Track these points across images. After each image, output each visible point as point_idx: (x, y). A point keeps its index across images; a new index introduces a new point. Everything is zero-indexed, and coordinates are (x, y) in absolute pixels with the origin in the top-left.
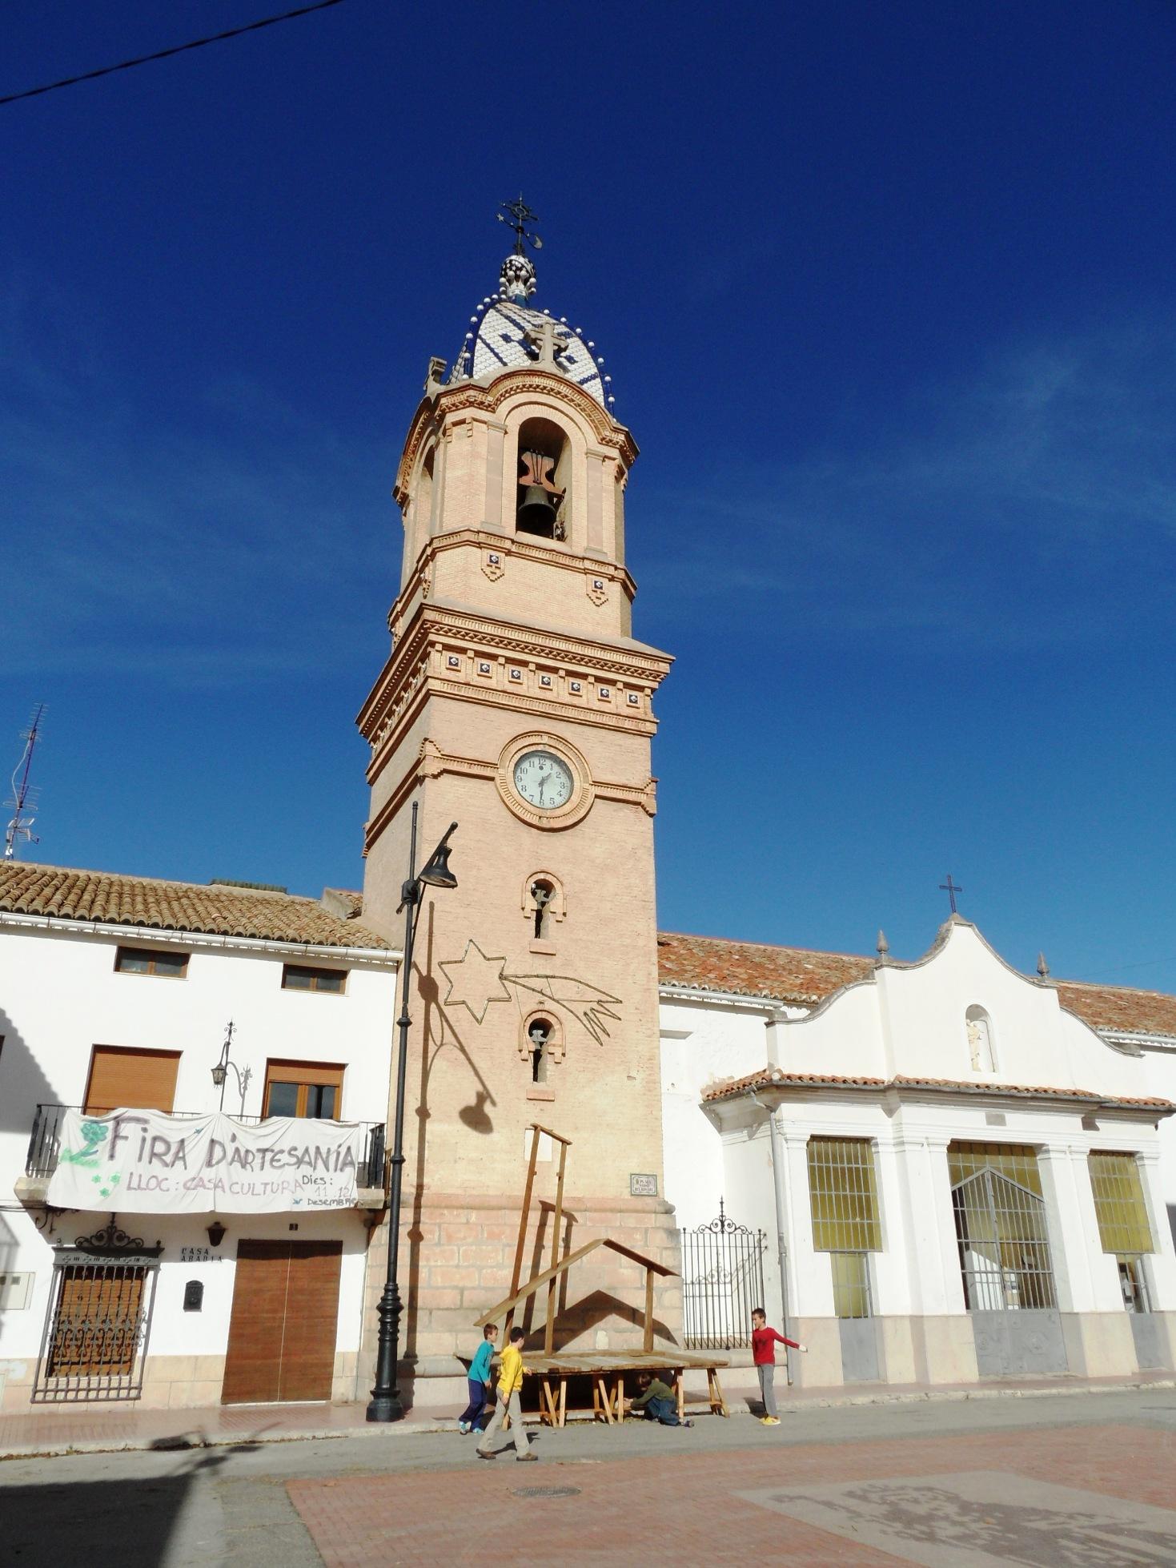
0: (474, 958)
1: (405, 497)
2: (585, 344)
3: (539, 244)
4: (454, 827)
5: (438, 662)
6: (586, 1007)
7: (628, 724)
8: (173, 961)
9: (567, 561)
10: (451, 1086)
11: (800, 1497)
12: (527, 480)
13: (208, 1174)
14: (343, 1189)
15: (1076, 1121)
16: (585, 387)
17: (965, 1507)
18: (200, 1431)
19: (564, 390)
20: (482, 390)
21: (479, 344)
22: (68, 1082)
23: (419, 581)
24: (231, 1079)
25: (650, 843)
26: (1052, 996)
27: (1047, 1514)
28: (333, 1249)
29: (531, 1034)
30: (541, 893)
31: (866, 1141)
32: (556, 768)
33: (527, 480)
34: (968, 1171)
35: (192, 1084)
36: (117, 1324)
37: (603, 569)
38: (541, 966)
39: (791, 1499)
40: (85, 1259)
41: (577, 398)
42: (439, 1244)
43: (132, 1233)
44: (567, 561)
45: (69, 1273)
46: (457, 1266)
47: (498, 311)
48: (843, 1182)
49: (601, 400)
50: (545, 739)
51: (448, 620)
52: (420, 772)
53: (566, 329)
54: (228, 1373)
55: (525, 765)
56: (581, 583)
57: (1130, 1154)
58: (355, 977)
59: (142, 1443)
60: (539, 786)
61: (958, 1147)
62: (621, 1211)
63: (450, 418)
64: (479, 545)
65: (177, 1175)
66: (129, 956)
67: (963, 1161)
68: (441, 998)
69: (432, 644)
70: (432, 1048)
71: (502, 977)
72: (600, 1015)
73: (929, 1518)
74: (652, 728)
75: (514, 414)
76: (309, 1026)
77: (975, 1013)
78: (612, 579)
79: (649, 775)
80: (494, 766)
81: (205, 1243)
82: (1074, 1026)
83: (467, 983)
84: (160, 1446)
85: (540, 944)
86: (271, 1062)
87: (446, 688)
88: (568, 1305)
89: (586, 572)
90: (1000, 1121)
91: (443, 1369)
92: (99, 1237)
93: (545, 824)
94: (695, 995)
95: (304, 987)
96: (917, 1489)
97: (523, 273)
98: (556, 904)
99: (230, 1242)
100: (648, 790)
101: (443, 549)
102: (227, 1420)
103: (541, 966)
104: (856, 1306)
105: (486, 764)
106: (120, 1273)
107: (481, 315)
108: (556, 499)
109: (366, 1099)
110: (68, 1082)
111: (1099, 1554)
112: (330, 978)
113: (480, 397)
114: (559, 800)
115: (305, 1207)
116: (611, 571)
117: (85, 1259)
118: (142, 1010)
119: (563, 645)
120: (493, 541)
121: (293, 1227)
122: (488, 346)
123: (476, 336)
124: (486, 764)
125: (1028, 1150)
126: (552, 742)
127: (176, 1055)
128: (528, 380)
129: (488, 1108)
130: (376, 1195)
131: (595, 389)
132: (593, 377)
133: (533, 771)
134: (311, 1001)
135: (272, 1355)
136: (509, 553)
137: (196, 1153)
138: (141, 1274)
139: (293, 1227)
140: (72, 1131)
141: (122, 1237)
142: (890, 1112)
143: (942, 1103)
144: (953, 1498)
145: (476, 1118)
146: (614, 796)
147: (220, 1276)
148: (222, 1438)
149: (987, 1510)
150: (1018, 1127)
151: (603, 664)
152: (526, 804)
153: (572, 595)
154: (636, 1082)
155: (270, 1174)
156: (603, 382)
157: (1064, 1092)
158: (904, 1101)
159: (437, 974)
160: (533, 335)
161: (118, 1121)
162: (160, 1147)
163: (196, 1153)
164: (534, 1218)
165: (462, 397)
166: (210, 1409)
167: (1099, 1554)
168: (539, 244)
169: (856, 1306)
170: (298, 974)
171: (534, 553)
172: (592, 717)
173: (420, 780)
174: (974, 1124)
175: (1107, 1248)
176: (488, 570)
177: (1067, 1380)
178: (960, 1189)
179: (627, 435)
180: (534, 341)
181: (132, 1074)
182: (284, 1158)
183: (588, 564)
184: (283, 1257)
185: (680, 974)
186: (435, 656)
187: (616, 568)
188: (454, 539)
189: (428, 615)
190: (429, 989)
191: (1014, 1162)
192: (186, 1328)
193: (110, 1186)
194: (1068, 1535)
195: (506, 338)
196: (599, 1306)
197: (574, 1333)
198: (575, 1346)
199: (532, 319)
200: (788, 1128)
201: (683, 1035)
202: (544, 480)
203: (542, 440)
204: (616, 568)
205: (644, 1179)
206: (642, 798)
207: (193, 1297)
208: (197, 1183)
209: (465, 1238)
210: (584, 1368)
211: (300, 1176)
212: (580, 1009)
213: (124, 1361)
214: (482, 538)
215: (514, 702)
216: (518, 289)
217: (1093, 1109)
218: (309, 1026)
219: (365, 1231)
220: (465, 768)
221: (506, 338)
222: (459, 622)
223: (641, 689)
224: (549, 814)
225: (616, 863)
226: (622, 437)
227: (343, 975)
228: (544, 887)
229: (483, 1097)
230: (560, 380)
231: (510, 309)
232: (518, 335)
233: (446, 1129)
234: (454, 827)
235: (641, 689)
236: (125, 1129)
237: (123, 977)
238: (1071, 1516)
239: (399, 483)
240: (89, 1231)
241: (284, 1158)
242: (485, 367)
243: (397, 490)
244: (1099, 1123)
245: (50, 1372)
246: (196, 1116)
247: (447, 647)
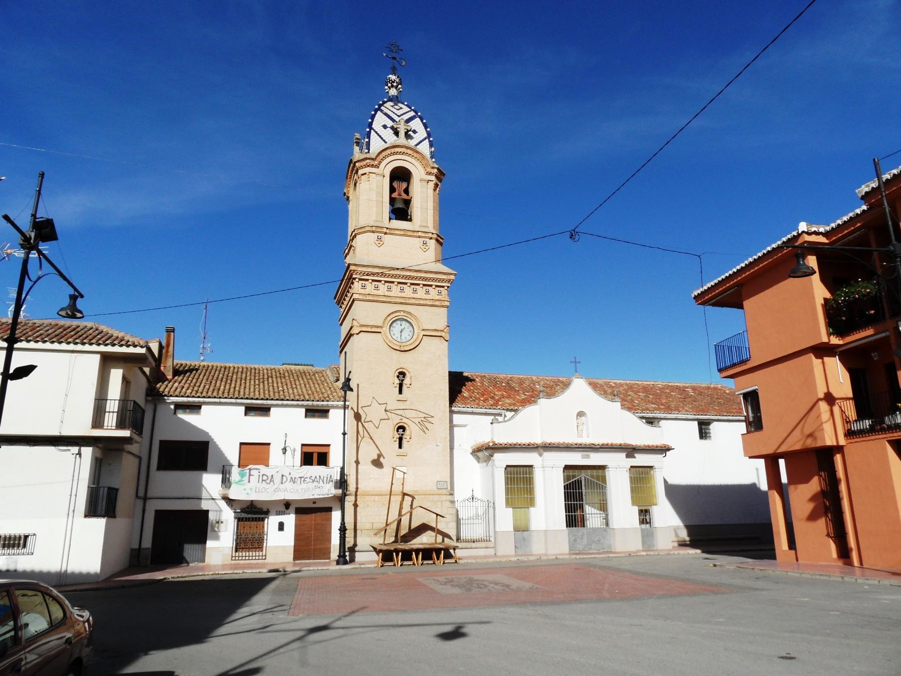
0: (375, 404)
1: (348, 198)
2: (422, 121)
3: (404, 63)
5: (357, 286)
6: (419, 420)
7: (437, 303)
8: (264, 411)
9: (411, 233)
10: (368, 453)
12: (395, 195)
13: (282, 486)
14: (329, 490)
15: (624, 455)
18: (284, 568)
19: (409, 152)
20: (372, 159)
22: (232, 456)
23: (351, 246)
24: (288, 452)
25: (446, 352)
28: (329, 510)
30: (401, 376)
31: (531, 466)
32: (408, 324)
33: (395, 195)
34: (574, 476)
35: (275, 453)
36: (257, 536)
37: (427, 235)
38: (401, 405)
40: (244, 515)
41: (415, 155)
43: (259, 506)
44: (411, 233)
45: (239, 520)
48: (520, 482)
50: (402, 313)
51: (360, 269)
52: (352, 332)
54: (295, 551)
55: (394, 325)
56: (418, 242)
57: (651, 467)
58: (332, 412)
59: (265, 570)
60: (401, 333)
61: (567, 468)
63: (360, 172)
64: (373, 232)
65: (271, 487)
66: (249, 410)
67: (571, 473)
68: (363, 420)
69: (355, 279)
70: (360, 439)
71: (386, 411)
72: (425, 422)
74: (447, 304)
75: (386, 168)
76: (319, 431)
77: (581, 414)
78: (431, 238)
80: (381, 327)
81: (283, 509)
83: (372, 414)
84: (270, 571)
85: (401, 397)
86: (303, 445)
87: (361, 297)
88: (412, 527)
89: (419, 237)
90: (588, 457)
91: (365, 549)
92: (248, 507)
94: (470, 410)
95: (313, 416)
97: (395, 84)
98: (407, 381)
99: (292, 509)
101: (359, 234)
102: (295, 565)
103: (401, 405)
104: (521, 529)
105: (378, 327)
106: (255, 520)
107: (373, 117)
108: (408, 202)
109: (335, 459)
110: (232, 456)
112: (323, 413)
113: (372, 162)
114: (409, 338)
115: (316, 497)
116: (430, 235)
117: (244, 515)
118: (256, 429)
121: (314, 503)
123: (371, 128)
124: (378, 327)
125: (603, 468)
127: (269, 444)
128: (393, 150)
129: (382, 459)
130: (340, 491)
132: (425, 139)
133: (397, 327)
134: (316, 422)
135: (309, 545)
136: (386, 233)
137: (277, 479)
138: (263, 520)
139: (314, 503)
140: (235, 472)
141: (256, 507)
142: (541, 455)
143: (561, 451)
145: (377, 463)
147: (290, 520)
148: (289, 569)
150: (595, 459)
151: (426, 279)
153: (412, 249)
155: (304, 486)
156: (430, 141)
158: (545, 451)
159: (360, 411)
161: (250, 470)
162: (265, 478)
163: (277, 479)
164: (396, 500)
165: (364, 163)
166: (289, 563)
168: (404, 63)
169: (521, 529)
170: (311, 412)
171: (397, 232)
173: (352, 335)
174: (576, 459)
175: (634, 503)
177: (611, 552)
179: (438, 169)
181: (254, 453)
182: (308, 480)
183: (420, 234)
184: (311, 513)
186: (356, 283)
188: (362, 230)
189: (352, 268)
190: (358, 417)
191: (595, 472)
192: (280, 538)
193: (249, 492)
195: (385, 127)
196: (424, 528)
197: (415, 537)
198: (415, 541)
200: (497, 463)
201: (465, 426)
202: (403, 193)
203: (401, 175)
206: (443, 334)
207: (281, 527)
208: (277, 490)
210: (414, 549)
211: (316, 485)
212: (417, 421)
213: (260, 548)
214: (374, 229)
215: (389, 300)
216: (393, 92)
217: (631, 451)
218: (319, 431)
221: (385, 127)
222: (364, 269)
223: (443, 287)
226: (436, 170)
227: (328, 411)
228: (402, 374)
229: (379, 456)
230: (407, 148)
233: (366, 467)
235: (443, 287)
236: (253, 472)
237: (247, 417)
239: (345, 191)
240: (244, 506)
241: (308, 480)
242: (376, 145)
243: (345, 194)
244: (636, 455)
245: (236, 551)
246: (277, 467)
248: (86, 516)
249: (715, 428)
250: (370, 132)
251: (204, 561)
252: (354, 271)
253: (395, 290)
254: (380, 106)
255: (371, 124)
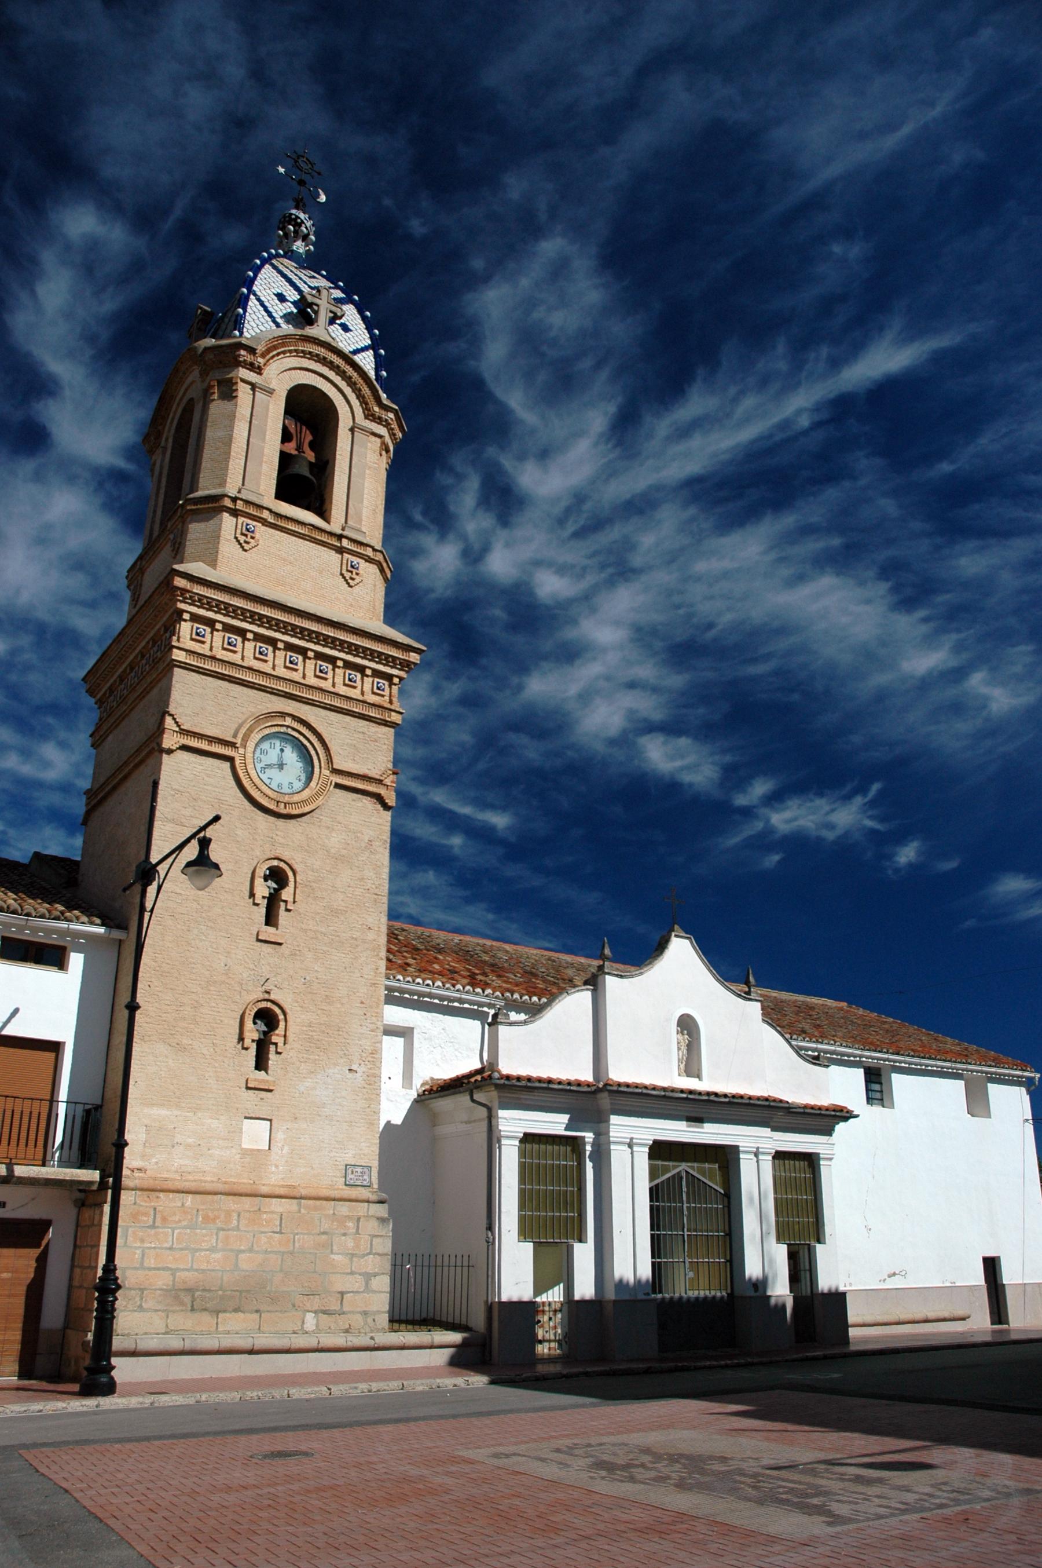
2: (361, 312)
3: (323, 198)
4: (217, 818)
7: (373, 713)
11: (514, 1454)
16: (357, 358)
17: (658, 1457)
21: (253, 302)
26: (755, 1009)
27: (724, 1459)
29: (255, 1023)
39: (507, 1456)
42: (153, 1226)
44: (324, 538)
46: (171, 1249)
47: (275, 267)
49: (372, 374)
51: (198, 589)
53: (342, 295)
62: (334, 1200)
73: (626, 1467)
79: (390, 766)
80: (233, 745)
82: (771, 1036)
93: (282, 810)
96: (614, 1445)
98: (286, 894)
100: (388, 782)
107: (257, 270)
111: (766, 1485)
119: (314, 627)
120: (251, 510)
122: (262, 304)
123: (250, 291)
126: (296, 725)
131: (367, 361)
144: (647, 1451)
146: (356, 785)
149: (673, 1459)
150: (712, 1133)
152: (264, 788)
154: (358, 1075)
156: (377, 356)
157: (758, 1098)
160: (310, 299)
167: (766, 1485)
168: (323, 198)
171: (291, 526)
172: (338, 703)
176: (242, 539)
178: (657, 1186)
180: (311, 305)
185: (404, 968)
187: (374, 550)
194: (742, 1474)
199: (313, 282)
204: (374, 550)
205: (359, 1170)
206: (382, 791)
209: (180, 1221)
219: (75, 1211)
220: (204, 745)
224: (287, 799)
225: (349, 854)
228: (277, 876)
231: (288, 266)
232: (293, 295)
234: (217, 818)
238: (743, 1460)
247: (195, 618)
248: (988, 1114)
249: (899, 1083)
250: (247, 299)
251: (55, 1047)
252: (184, 591)
253: (277, 662)
254: (271, 257)
255: (252, 281)
